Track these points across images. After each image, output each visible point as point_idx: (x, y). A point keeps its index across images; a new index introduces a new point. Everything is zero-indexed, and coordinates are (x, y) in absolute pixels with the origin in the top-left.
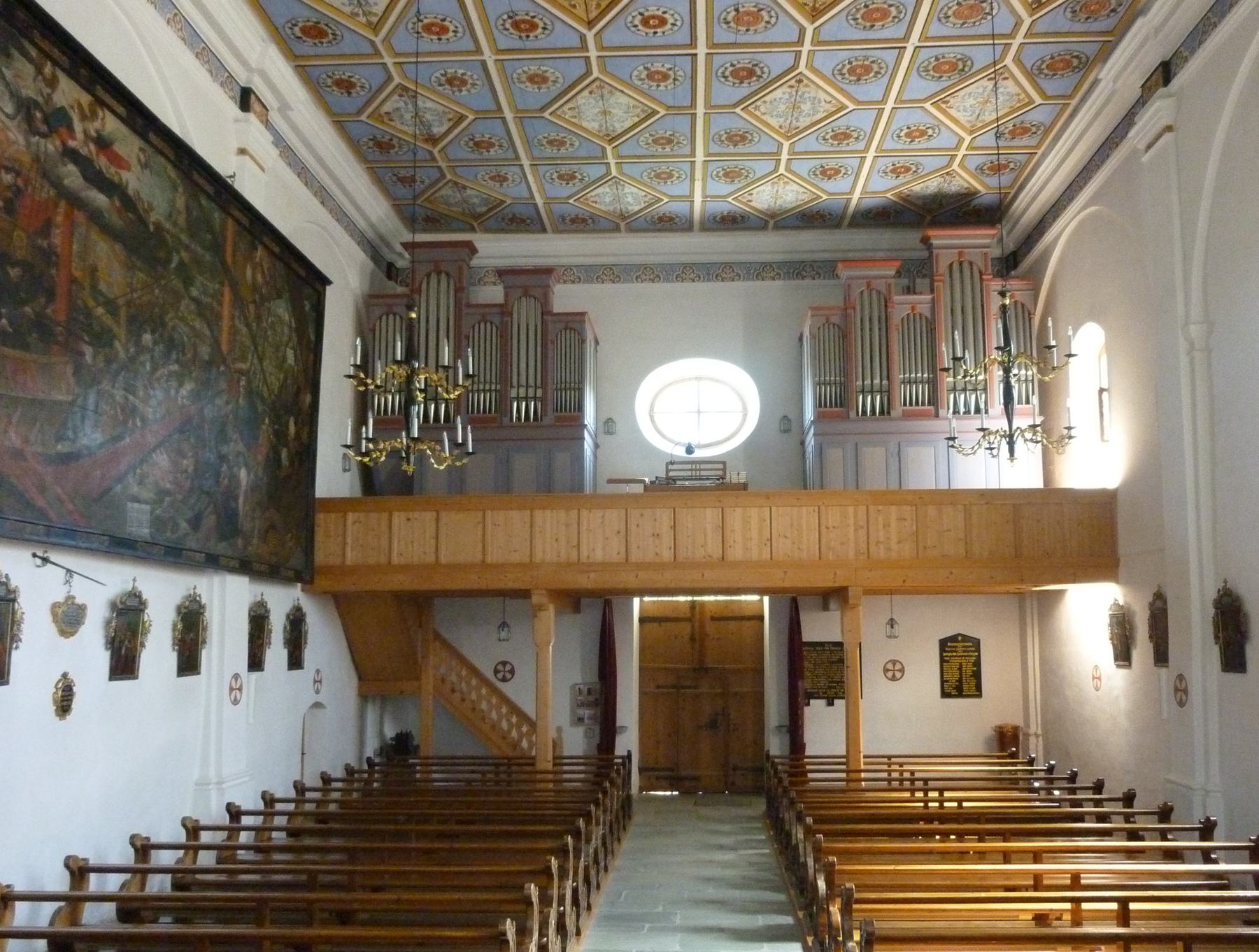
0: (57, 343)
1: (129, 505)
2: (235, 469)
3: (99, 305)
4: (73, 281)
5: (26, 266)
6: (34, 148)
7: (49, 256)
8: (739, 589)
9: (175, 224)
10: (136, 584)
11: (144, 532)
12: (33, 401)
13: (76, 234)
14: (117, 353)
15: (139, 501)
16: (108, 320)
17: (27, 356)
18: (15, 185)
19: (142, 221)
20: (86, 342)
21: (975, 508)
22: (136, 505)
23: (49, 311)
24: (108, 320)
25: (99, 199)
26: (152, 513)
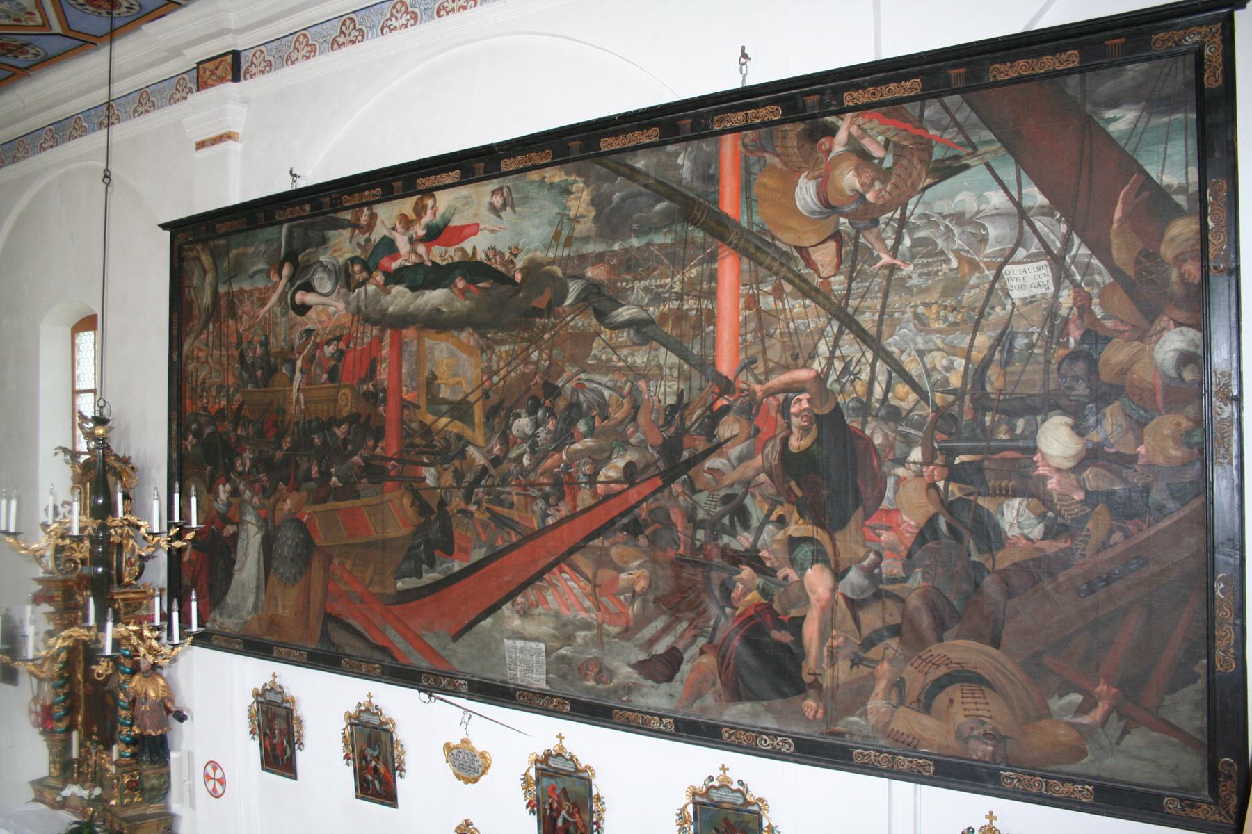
0: (392, 479)
1: (508, 643)
2: (883, 544)
3: (440, 415)
4: (405, 405)
5: (353, 419)
6: (354, 304)
7: (373, 397)
8: (201, 85)
9: (1166, 64)
10: (564, 743)
11: (538, 680)
12: (368, 546)
13: (406, 355)
14: (474, 460)
15: (524, 638)
16: (456, 427)
17: (357, 503)
18: (613, 268)
19: (503, 279)
20: (426, 465)
21: (934, 316)
22: (519, 643)
23: (378, 450)
24: (456, 427)
25: (435, 297)
26: (548, 653)
